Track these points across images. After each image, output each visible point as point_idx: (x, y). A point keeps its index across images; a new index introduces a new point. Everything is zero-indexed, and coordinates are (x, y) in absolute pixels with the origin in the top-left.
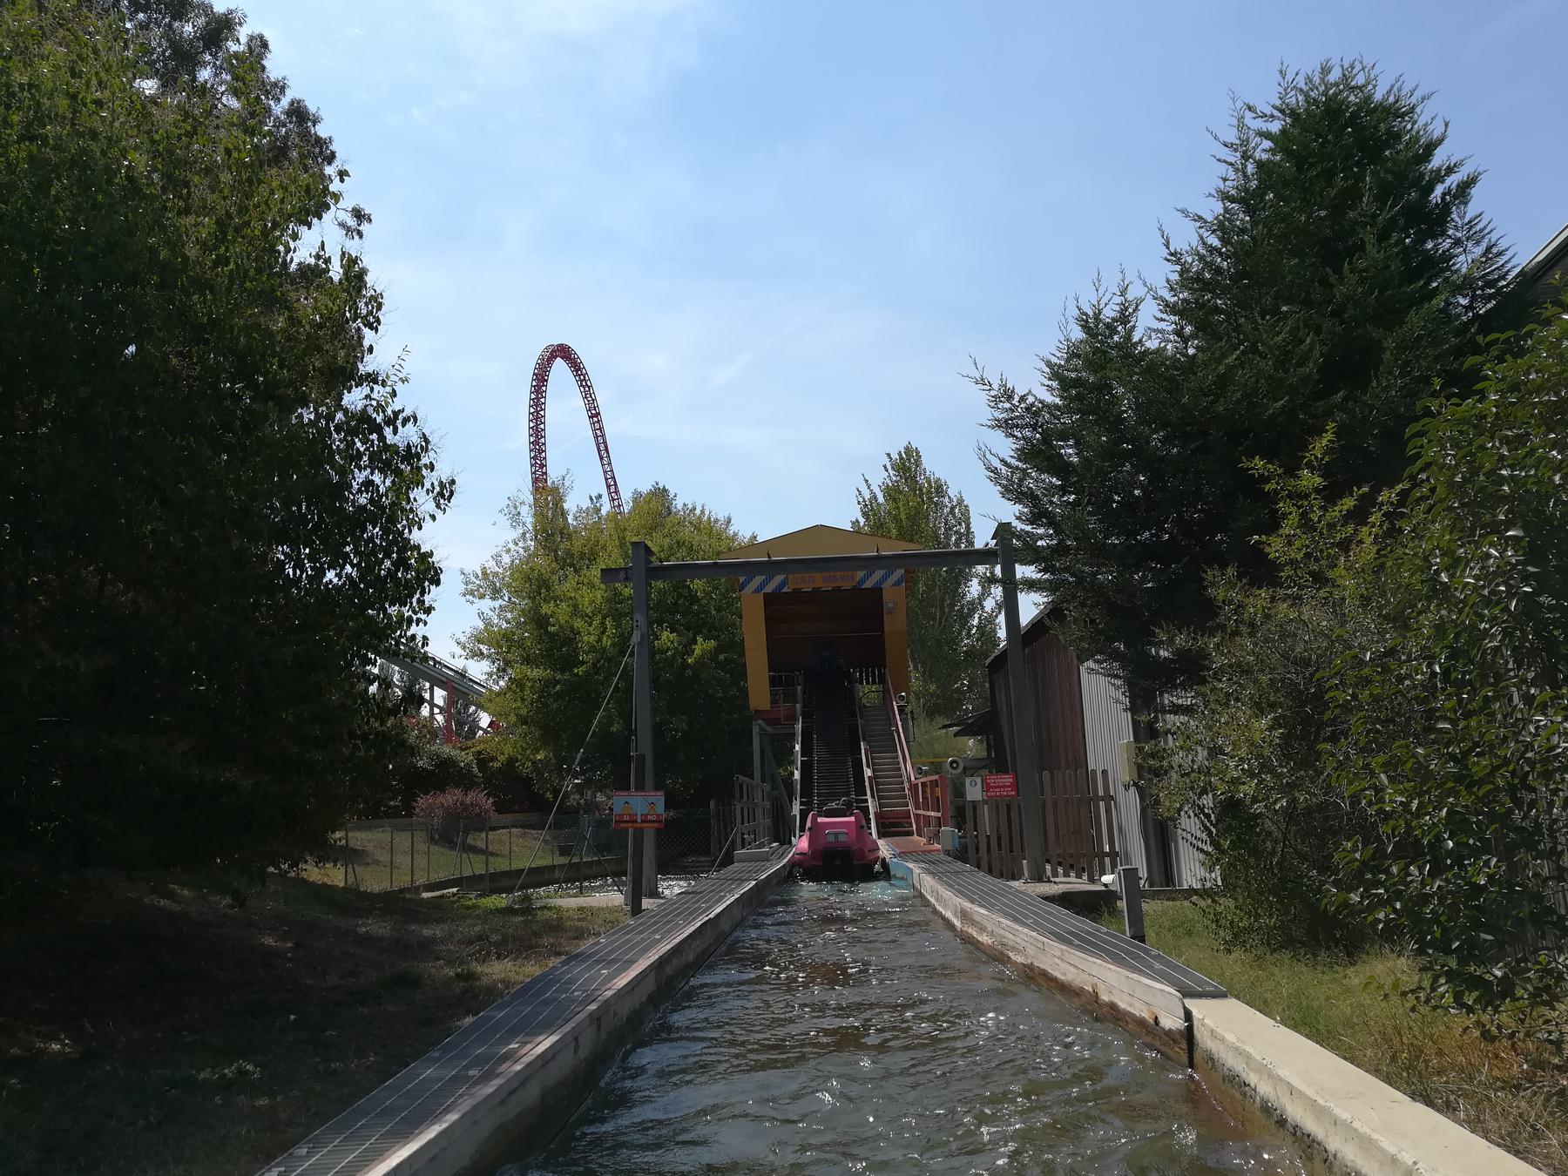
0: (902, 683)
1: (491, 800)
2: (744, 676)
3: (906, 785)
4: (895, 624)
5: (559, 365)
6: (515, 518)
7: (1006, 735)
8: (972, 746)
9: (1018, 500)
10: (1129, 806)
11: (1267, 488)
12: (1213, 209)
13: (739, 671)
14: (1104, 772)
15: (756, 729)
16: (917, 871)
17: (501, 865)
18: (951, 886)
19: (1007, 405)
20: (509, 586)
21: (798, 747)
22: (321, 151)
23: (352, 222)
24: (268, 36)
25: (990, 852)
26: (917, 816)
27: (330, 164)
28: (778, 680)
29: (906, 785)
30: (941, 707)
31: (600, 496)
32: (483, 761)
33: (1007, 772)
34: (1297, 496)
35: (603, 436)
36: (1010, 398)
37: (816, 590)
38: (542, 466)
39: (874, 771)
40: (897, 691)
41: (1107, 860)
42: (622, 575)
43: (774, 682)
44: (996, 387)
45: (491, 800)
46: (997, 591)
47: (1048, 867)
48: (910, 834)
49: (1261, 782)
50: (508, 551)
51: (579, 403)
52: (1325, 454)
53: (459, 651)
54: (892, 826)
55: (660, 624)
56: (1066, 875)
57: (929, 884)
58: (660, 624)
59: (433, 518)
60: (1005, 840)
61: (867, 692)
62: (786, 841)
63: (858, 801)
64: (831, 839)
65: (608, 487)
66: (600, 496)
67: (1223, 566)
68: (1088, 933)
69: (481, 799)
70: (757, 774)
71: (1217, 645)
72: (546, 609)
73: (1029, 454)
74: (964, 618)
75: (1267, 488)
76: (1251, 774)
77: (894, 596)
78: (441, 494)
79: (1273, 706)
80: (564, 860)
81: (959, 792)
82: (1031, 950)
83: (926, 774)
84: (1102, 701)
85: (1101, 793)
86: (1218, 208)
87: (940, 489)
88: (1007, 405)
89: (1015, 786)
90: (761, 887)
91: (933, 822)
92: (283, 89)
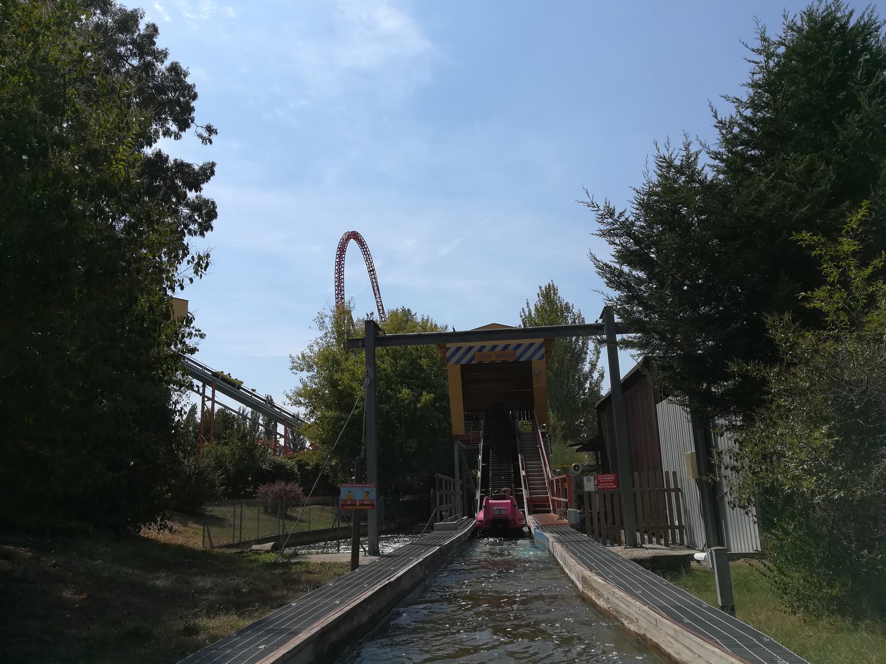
0: (545, 419)
1: (301, 489)
2: (450, 416)
3: (547, 481)
4: (539, 383)
5: (352, 243)
6: (322, 325)
7: (608, 450)
8: (587, 458)
9: (618, 288)
10: (692, 496)
11: (814, 253)
12: (745, 94)
13: (446, 412)
14: (674, 473)
15: (456, 446)
16: (551, 540)
17: (305, 527)
18: (575, 554)
19: (610, 220)
20: (317, 364)
21: (480, 457)
22: (190, 93)
23: (206, 135)
24: (157, 25)
25: (599, 524)
26: (553, 501)
27: (194, 100)
28: (470, 418)
29: (547, 481)
30: (570, 434)
31: (372, 314)
32: (301, 466)
33: (609, 473)
34: (836, 259)
35: (376, 282)
36: (612, 214)
37: (492, 363)
38: (342, 298)
39: (526, 472)
40: (541, 423)
41: (677, 531)
42: (360, 343)
43: (467, 418)
44: (602, 208)
45: (301, 489)
46: (604, 350)
47: (638, 534)
48: (549, 512)
49: (819, 478)
50: (318, 343)
51: (364, 267)
52: (859, 226)
53: (288, 401)
54: (537, 507)
55: (401, 385)
56: (651, 542)
57: (559, 550)
58: (401, 385)
59: (191, 280)
60: (610, 517)
61: (523, 425)
62: (472, 516)
63: (516, 491)
64: (497, 513)
65: (379, 310)
66: (372, 314)
67: (781, 313)
68: (693, 609)
69: (296, 488)
70: (457, 474)
71: (778, 374)
72: (337, 376)
73: (624, 256)
74: (581, 385)
75: (814, 253)
76: (808, 472)
77: (538, 366)
78: (198, 264)
79: (826, 420)
80: (343, 525)
81: (580, 485)
82: (643, 623)
83: (559, 474)
84: (673, 421)
85: (672, 487)
86: (751, 91)
87: (567, 308)
88: (610, 220)
89: (616, 482)
90: (443, 551)
91: (563, 505)
92: (166, 55)
